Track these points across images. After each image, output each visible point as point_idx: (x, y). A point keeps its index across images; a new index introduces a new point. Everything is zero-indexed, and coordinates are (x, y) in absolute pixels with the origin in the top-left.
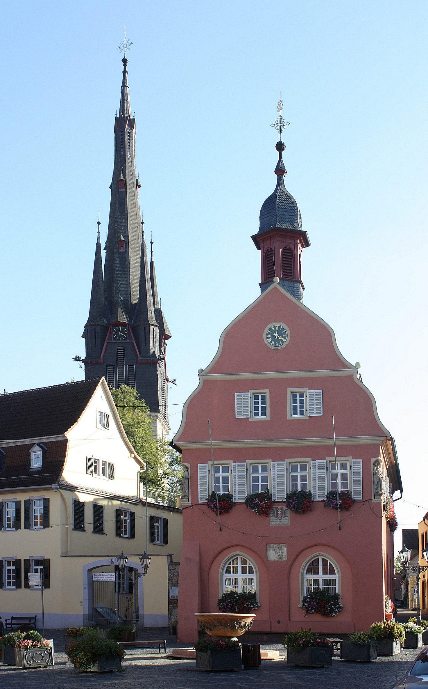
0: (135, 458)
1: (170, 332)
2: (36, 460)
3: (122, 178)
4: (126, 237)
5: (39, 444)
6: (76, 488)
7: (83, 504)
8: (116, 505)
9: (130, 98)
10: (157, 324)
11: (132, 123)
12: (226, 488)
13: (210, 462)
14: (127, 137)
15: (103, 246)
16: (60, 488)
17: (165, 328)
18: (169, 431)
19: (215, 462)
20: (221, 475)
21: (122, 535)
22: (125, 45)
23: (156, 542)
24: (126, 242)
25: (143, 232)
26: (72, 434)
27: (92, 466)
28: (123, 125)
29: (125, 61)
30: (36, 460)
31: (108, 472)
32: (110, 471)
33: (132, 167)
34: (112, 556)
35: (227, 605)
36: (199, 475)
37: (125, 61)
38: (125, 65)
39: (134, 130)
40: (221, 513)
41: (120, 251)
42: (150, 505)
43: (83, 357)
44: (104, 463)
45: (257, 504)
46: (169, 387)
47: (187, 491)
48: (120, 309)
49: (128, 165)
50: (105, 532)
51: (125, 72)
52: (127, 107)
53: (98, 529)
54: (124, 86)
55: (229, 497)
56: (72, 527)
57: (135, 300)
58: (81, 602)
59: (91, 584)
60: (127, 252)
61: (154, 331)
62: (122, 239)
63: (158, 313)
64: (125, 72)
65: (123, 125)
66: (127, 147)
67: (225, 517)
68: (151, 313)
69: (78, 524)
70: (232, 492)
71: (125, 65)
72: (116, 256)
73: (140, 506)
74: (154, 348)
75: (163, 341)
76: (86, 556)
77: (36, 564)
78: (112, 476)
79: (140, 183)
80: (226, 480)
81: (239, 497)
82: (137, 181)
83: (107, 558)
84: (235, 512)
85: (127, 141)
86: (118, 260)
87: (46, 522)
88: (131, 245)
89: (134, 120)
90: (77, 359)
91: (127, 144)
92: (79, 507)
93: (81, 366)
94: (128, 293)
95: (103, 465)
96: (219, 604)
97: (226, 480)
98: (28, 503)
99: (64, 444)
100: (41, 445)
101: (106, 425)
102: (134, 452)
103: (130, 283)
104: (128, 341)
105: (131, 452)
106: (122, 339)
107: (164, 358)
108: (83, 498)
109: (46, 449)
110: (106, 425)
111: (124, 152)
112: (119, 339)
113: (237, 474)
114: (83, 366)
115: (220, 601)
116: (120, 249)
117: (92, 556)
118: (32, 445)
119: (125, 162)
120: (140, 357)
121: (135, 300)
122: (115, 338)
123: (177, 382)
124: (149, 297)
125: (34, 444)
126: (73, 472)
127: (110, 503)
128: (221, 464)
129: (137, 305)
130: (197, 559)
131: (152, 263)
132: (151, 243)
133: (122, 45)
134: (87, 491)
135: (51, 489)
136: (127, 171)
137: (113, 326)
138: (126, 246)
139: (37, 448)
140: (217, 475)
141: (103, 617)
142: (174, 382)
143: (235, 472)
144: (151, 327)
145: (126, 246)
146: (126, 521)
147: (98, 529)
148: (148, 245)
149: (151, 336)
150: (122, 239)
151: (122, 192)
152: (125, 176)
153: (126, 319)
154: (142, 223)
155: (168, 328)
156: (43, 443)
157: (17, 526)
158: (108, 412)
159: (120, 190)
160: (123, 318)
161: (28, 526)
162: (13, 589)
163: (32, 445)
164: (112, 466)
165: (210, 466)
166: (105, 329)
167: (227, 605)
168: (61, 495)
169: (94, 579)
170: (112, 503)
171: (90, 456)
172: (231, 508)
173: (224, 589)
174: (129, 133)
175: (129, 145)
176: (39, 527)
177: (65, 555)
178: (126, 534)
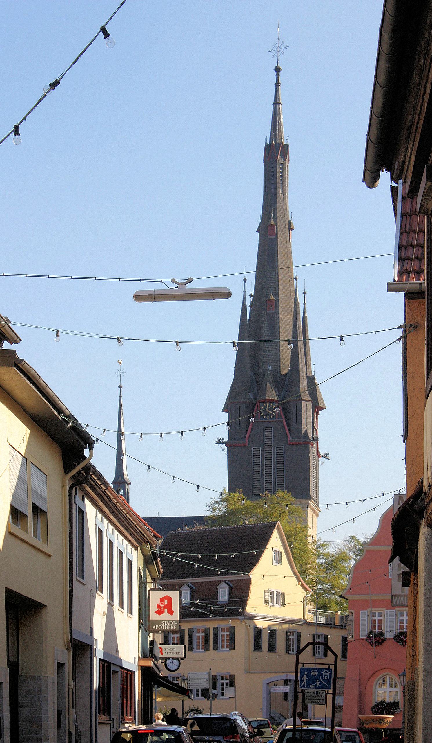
0: (302, 586)
1: (324, 404)
2: (223, 594)
3: (272, 222)
4: (276, 295)
5: (225, 582)
6: (255, 617)
7: (261, 630)
8: (286, 628)
9: (283, 118)
10: (310, 399)
11: (285, 150)
12: (380, 628)
13: (369, 609)
14: (279, 170)
15: (248, 303)
16: (245, 619)
17: (319, 398)
18: (320, 513)
19: (373, 609)
20: (377, 618)
21: (290, 652)
22: (278, 49)
23: (317, 655)
24: (276, 301)
25: (296, 290)
26: (255, 574)
27: (268, 597)
28: (275, 154)
29: (278, 70)
30: (223, 594)
31: (280, 601)
32: (281, 599)
33: (285, 207)
34: (287, 672)
35: (378, 710)
36: (361, 618)
37: (278, 70)
38: (278, 75)
39: (287, 159)
40: (376, 646)
41: (268, 312)
42: (312, 624)
43: (226, 439)
44: (278, 593)
45: (402, 640)
46: (320, 463)
47: (352, 630)
48: (268, 384)
49: (279, 205)
50: (277, 651)
51: (277, 85)
52: (280, 130)
53: (272, 648)
54: (276, 103)
55: (382, 634)
56: (253, 649)
57: (285, 369)
58: (261, 709)
59: (269, 693)
60: (277, 313)
61: (307, 406)
62: (272, 297)
63: (311, 380)
64: (277, 85)
65: (275, 154)
66: (279, 182)
67: (379, 648)
68: (304, 385)
69: (258, 647)
70: (384, 629)
71: (278, 75)
72: (264, 318)
73: (305, 626)
74: (306, 427)
75: (315, 414)
76: (265, 673)
77: (222, 678)
78: (283, 604)
79: (294, 224)
80: (380, 622)
81: (389, 635)
82: (290, 222)
83: (283, 674)
84: (385, 644)
85: (279, 174)
86: (266, 323)
87: (232, 645)
88: (282, 304)
89: (287, 146)
90: (219, 442)
91: (279, 178)
92: (258, 632)
93: (223, 450)
94: (277, 362)
95: (277, 594)
96: (372, 710)
97: (380, 622)
98: (216, 630)
99: (248, 581)
100: (227, 581)
101: (279, 561)
102: (302, 580)
103: (280, 350)
104: (277, 420)
105: (299, 581)
106: (270, 418)
107: (317, 440)
108: (261, 624)
109: (232, 585)
110: (279, 561)
111: (276, 189)
112: (266, 418)
113: (388, 618)
114: (226, 448)
115: (373, 708)
116: (269, 310)
117: (271, 673)
118: (221, 582)
119: (275, 201)
120: (290, 438)
121: (285, 369)
122: (262, 417)
123: (330, 456)
124: (302, 367)
125: (222, 581)
126: (254, 604)
127: (280, 628)
128: (377, 611)
129: (288, 376)
130: (358, 679)
131: (304, 318)
132: (304, 293)
133: (275, 49)
134: (264, 618)
135: (238, 619)
136: (279, 213)
137: (260, 402)
138: (276, 306)
139: (224, 584)
140: (374, 618)
141: (275, 720)
142: (326, 456)
143: (387, 616)
144: (304, 403)
145: (276, 306)
146: (293, 639)
147: (272, 648)
148: (300, 300)
149: (304, 413)
150: (272, 297)
151: (272, 239)
152: (276, 219)
153: (275, 395)
154: (296, 279)
155: (322, 399)
156: (229, 581)
157: (207, 649)
158: (282, 549)
159: (269, 237)
160: (272, 394)
161: (215, 648)
162: (202, 699)
163: (221, 582)
164: (283, 594)
165: (369, 612)
166: (252, 407)
167: (378, 710)
168: (245, 623)
169: (271, 691)
170: (282, 628)
171: (267, 589)
172: (383, 642)
173: (376, 700)
174: (281, 164)
175: (282, 180)
176: (225, 649)
177: (248, 672)
178: (293, 651)
